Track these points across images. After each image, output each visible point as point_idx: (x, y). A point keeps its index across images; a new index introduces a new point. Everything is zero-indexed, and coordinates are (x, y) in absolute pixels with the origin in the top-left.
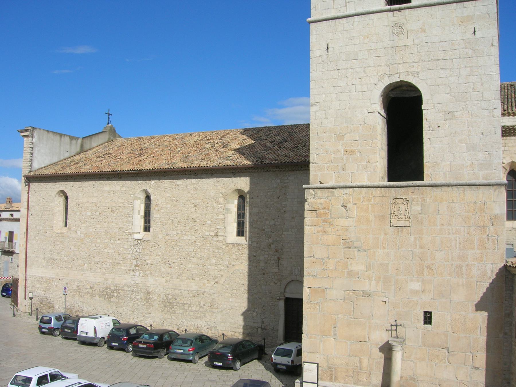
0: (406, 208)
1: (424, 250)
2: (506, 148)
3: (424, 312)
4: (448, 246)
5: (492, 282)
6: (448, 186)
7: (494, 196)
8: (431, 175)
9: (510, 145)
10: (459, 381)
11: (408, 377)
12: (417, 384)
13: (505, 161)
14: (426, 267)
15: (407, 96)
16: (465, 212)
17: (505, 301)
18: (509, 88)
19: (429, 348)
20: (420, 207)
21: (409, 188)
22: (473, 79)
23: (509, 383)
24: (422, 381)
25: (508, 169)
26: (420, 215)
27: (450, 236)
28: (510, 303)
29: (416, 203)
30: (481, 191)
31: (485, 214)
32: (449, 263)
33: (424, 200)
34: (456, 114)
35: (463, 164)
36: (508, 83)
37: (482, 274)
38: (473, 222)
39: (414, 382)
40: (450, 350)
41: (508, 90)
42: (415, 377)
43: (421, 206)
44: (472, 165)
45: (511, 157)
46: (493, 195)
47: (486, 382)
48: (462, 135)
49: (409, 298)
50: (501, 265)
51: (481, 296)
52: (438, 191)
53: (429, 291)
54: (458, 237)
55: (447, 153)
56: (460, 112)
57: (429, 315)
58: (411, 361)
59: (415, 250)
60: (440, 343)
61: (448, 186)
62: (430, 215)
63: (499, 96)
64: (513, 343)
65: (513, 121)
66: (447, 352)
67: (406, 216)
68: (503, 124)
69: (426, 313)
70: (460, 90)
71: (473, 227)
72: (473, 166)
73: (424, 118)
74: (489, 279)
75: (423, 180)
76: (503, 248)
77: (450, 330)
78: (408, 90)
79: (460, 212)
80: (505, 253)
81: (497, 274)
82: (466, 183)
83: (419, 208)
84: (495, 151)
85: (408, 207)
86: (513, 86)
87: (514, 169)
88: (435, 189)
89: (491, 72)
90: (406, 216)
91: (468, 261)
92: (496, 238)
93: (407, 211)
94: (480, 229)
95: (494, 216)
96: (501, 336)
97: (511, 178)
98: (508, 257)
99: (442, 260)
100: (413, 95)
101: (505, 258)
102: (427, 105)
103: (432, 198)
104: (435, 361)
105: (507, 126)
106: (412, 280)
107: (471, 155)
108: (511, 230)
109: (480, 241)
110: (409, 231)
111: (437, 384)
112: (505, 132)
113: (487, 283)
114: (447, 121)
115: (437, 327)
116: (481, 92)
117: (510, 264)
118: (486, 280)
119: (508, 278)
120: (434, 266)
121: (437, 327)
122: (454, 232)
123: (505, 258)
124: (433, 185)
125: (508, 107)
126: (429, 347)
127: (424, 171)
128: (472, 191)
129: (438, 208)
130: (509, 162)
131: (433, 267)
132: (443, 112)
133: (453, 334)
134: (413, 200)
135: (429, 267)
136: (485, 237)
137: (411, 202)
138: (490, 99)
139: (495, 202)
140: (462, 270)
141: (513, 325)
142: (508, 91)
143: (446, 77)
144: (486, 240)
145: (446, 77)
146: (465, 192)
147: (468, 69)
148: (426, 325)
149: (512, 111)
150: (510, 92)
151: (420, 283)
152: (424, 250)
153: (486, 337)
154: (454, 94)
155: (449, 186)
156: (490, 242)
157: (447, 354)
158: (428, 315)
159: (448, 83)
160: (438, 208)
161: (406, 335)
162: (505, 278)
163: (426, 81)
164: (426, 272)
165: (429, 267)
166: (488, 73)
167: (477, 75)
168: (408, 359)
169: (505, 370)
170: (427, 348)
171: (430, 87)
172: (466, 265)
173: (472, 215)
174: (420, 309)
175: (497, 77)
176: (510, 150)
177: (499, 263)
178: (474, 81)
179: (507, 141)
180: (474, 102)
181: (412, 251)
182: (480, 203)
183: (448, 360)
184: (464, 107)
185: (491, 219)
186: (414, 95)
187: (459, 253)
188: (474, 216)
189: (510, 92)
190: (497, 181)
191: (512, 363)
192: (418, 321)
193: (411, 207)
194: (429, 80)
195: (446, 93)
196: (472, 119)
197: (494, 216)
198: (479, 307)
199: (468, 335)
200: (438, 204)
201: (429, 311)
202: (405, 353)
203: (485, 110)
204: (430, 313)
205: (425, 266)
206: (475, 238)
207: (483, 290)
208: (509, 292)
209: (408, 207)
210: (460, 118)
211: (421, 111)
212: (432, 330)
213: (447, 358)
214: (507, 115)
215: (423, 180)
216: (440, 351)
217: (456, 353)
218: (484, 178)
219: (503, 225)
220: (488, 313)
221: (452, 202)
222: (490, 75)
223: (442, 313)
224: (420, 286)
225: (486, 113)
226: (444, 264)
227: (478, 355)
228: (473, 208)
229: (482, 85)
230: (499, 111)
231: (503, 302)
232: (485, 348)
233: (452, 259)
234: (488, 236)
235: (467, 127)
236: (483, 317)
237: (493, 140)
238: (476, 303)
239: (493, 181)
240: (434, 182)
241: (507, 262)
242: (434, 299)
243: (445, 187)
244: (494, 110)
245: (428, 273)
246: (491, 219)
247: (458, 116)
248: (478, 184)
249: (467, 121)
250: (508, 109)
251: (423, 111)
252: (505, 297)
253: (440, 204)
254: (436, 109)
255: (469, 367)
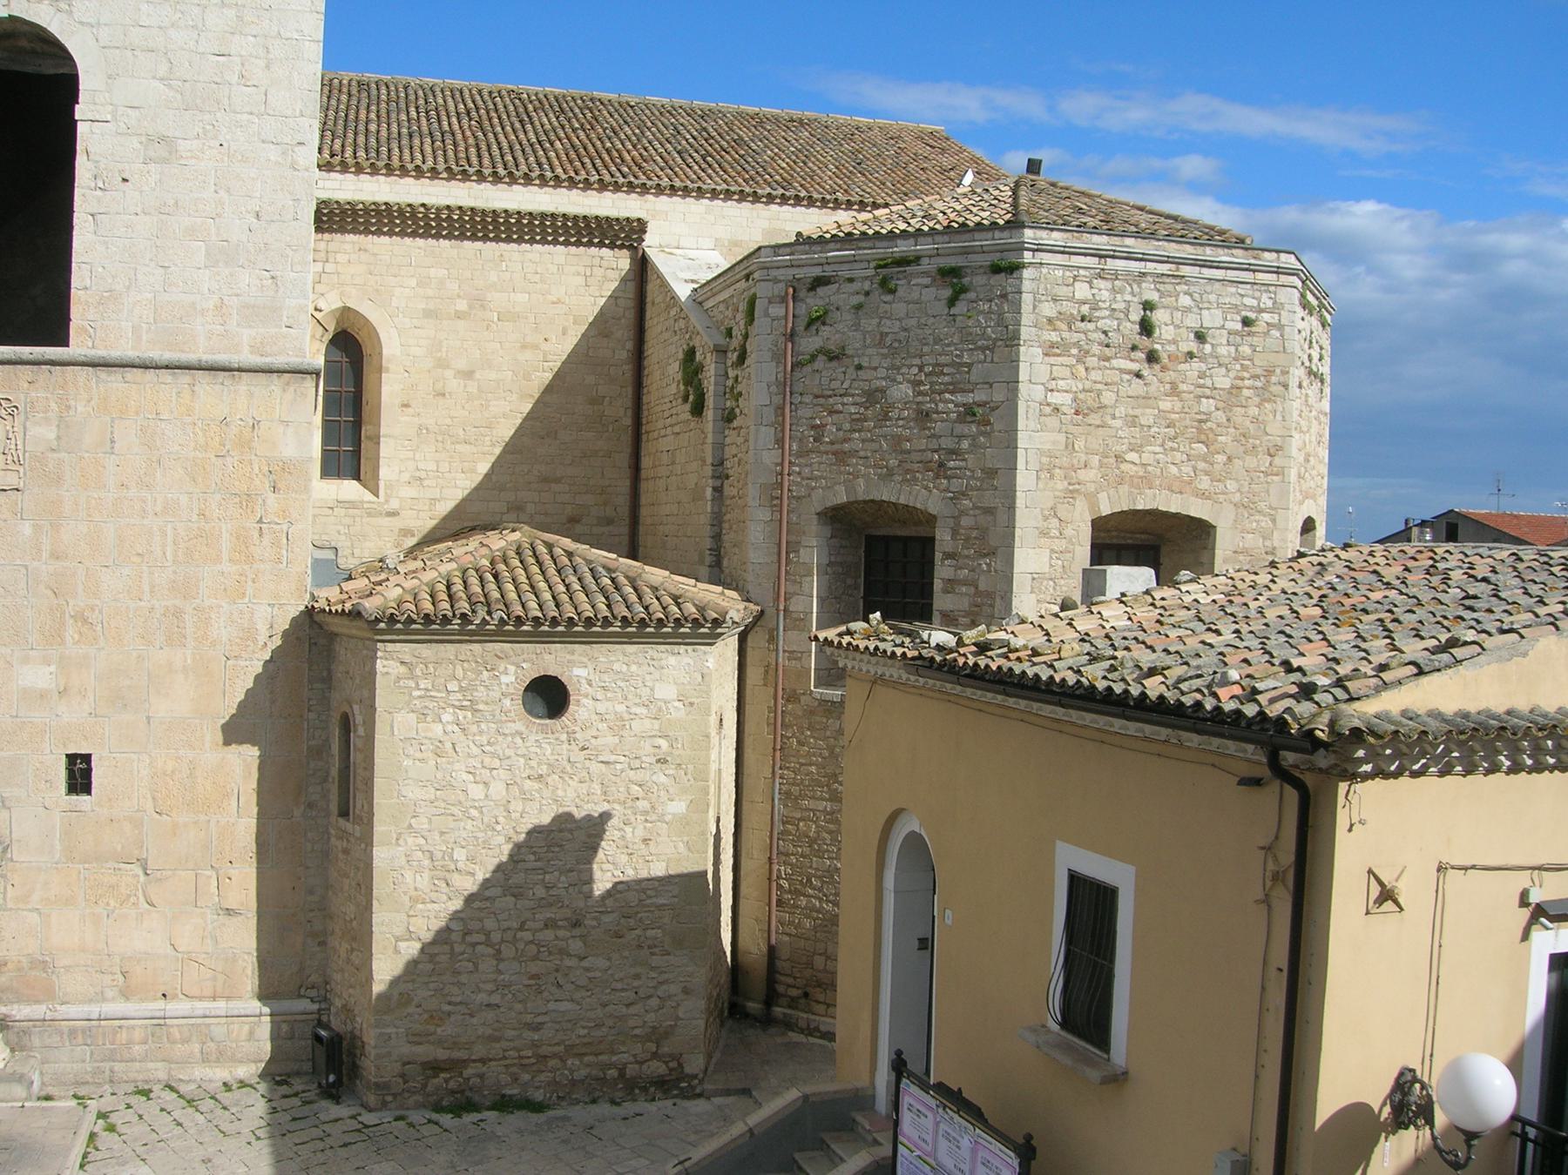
0: (8, 431)
1: (65, 564)
2: (329, 267)
3: (68, 756)
4: (140, 552)
5: (272, 657)
6: (145, 366)
7: (281, 404)
8: (91, 330)
9: (341, 258)
10: (180, 955)
11: (24, 960)
12: (54, 977)
13: (321, 305)
14: (72, 617)
15: (29, 69)
16: (195, 449)
17: (309, 711)
18: (354, 91)
19: (87, 866)
20: (54, 428)
21: (19, 366)
22: (242, 47)
23: (323, 944)
24: (70, 967)
25: (332, 328)
26: (55, 455)
27: (145, 522)
28: (324, 717)
29: (42, 415)
30: (245, 388)
31: (253, 457)
32: (142, 603)
33: (69, 407)
34: (183, 146)
35: (193, 303)
36: (352, 75)
37: (241, 635)
38: (219, 482)
39: (45, 975)
40: (151, 865)
41: (350, 95)
42: (47, 959)
43: (58, 426)
44: (221, 305)
45: (342, 294)
46: (278, 401)
47: (258, 950)
48: (196, 214)
49: (17, 717)
50: (296, 608)
51: (239, 700)
52: (113, 381)
53: (82, 690)
54: (169, 526)
55: (148, 266)
56: (195, 141)
57: (84, 766)
58: (30, 910)
59: (35, 564)
60: (119, 848)
61: (145, 366)
62: (86, 455)
63: (315, 107)
64: (333, 832)
65: (353, 188)
66: (141, 873)
67: (10, 457)
68: (324, 195)
69: (72, 758)
70: (199, 74)
71: (218, 497)
72: (224, 310)
73: (79, 147)
74: (261, 649)
75: (65, 343)
76: (303, 559)
77: (149, 805)
78: (34, 52)
79: (177, 448)
80: (309, 572)
81: (286, 634)
82: (200, 361)
83: (50, 434)
84: (292, 271)
85: (15, 429)
86: (365, 87)
87: (349, 330)
88: (102, 373)
89: (297, 31)
90: (10, 457)
91: (200, 596)
92: (285, 527)
93: (13, 441)
94: (237, 500)
95: (281, 464)
96: (297, 813)
97: (338, 356)
98: (318, 584)
99: (121, 596)
100: (49, 68)
101: (309, 586)
102: (92, 107)
103: (93, 403)
104: (108, 904)
105: (337, 202)
106: (26, 660)
107: (218, 278)
108: (332, 508)
109: (238, 539)
110: (17, 504)
111: (117, 969)
112: (328, 220)
113: (256, 662)
114: (152, 167)
115: (110, 800)
116: (263, 89)
117: (322, 604)
118: (254, 652)
119: (315, 644)
120: (97, 612)
121: (110, 800)
122: (158, 509)
123: (309, 586)
124: (96, 361)
125: (343, 146)
126: (85, 863)
127: (73, 316)
128: (218, 387)
129: (112, 433)
130: (334, 307)
131: (94, 617)
132: (141, 135)
133: (157, 816)
134: (33, 407)
135: (81, 618)
136: (252, 525)
137: (26, 412)
138: (289, 113)
139: (286, 423)
140: (181, 625)
141: (331, 780)
142: (349, 101)
143: (160, 27)
144: (256, 535)
145: (160, 27)
146: (196, 388)
147: (231, 13)
148: (74, 797)
149: (355, 158)
150: (354, 102)
151: (53, 668)
152: (65, 564)
153: (255, 821)
154: (180, 83)
155: (147, 367)
156: (266, 540)
157: (142, 878)
158: (81, 766)
159: (166, 47)
160: (112, 433)
161: (11, 832)
162: (307, 645)
163: (94, 30)
164: (71, 633)
165: (81, 618)
166: (289, 35)
167: (255, 36)
168: (21, 906)
169: (312, 911)
170: (81, 866)
171: (105, 50)
172: (195, 609)
173: (214, 459)
174: (53, 746)
175: (313, 54)
176: (339, 273)
177: (293, 602)
178: (243, 53)
179: (332, 246)
180: (239, 115)
181: (26, 567)
182: (242, 423)
183: (145, 896)
184: (208, 127)
185: (270, 472)
186: (52, 71)
187: (175, 572)
188: (220, 460)
189: (354, 102)
190: (293, 360)
191: (332, 886)
192: (48, 785)
193: (25, 428)
194: (106, 28)
195: (154, 78)
196: (229, 166)
197: (281, 464)
198: (234, 732)
199: (203, 818)
200: (112, 421)
201: (83, 752)
202: (9, 887)
203: (272, 147)
204: (87, 758)
205: (67, 615)
206: (221, 528)
207: (245, 682)
208: (319, 686)
209: (15, 429)
210: (193, 162)
211: (72, 125)
212: (93, 811)
213: (144, 892)
214: (338, 168)
215: (68, 346)
216: (118, 872)
217: (170, 873)
218: (254, 349)
219: (306, 489)
220: (259, 749)
221: (154, 416)
222: (294, 42)
223: (123, 755)
224: (54, 676)
225: (273, 154)
226: (127, 608)
227: (233, 872)
228: (217, 439)
229: (268, 67)
230: (309, 155)
231: (301, 716)
232: (254, 851)
233: (151, 592)
234: (260, 521)
235: (213, 190)
236: (247, 757)
237: (288, 238)
238: (223, 721)
239: (280, 361)
240: (100, 353)
241: (313, 598)
242: (96, 716)
243: (135, 370)
244: (296, 149)
245: (76, 636)
246: (270, 472)
247: (189, 154)
248: (236, 366)
249: (213, 172)
250: (343, 152)
251: (79, 123)
252: (309, 700)
253: (116, 422)
254: (122, 124)
255: (209, 911)
